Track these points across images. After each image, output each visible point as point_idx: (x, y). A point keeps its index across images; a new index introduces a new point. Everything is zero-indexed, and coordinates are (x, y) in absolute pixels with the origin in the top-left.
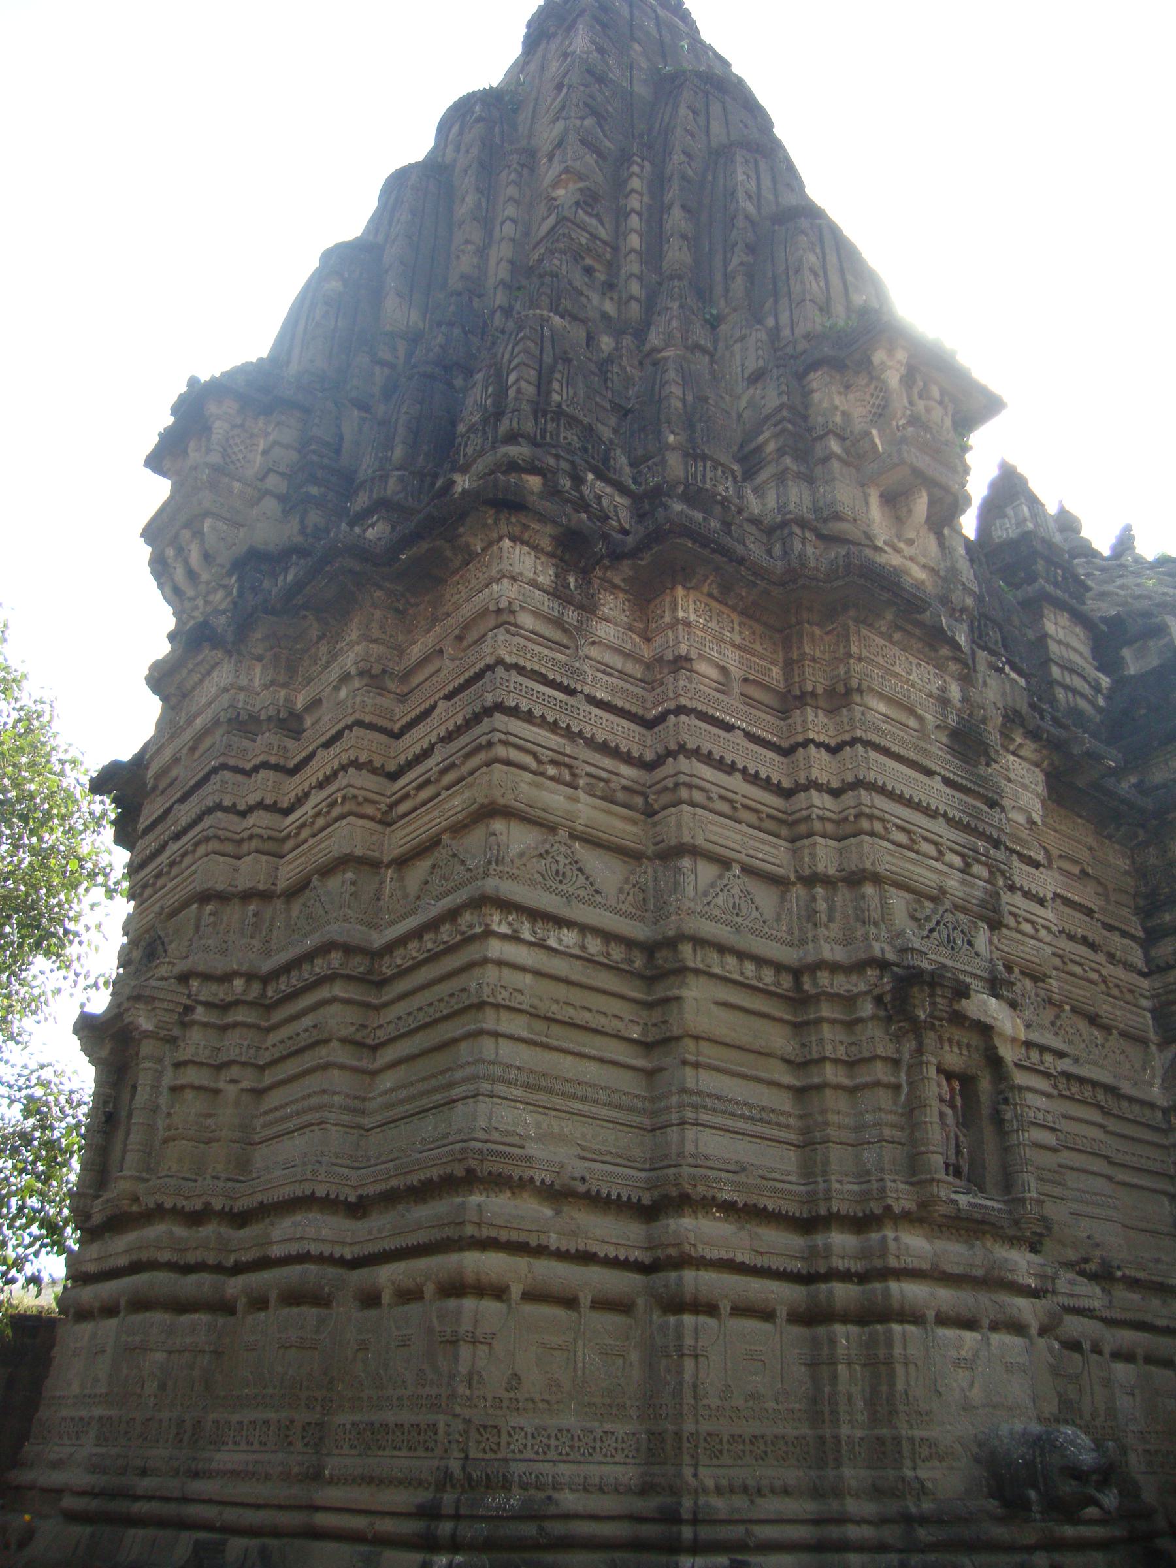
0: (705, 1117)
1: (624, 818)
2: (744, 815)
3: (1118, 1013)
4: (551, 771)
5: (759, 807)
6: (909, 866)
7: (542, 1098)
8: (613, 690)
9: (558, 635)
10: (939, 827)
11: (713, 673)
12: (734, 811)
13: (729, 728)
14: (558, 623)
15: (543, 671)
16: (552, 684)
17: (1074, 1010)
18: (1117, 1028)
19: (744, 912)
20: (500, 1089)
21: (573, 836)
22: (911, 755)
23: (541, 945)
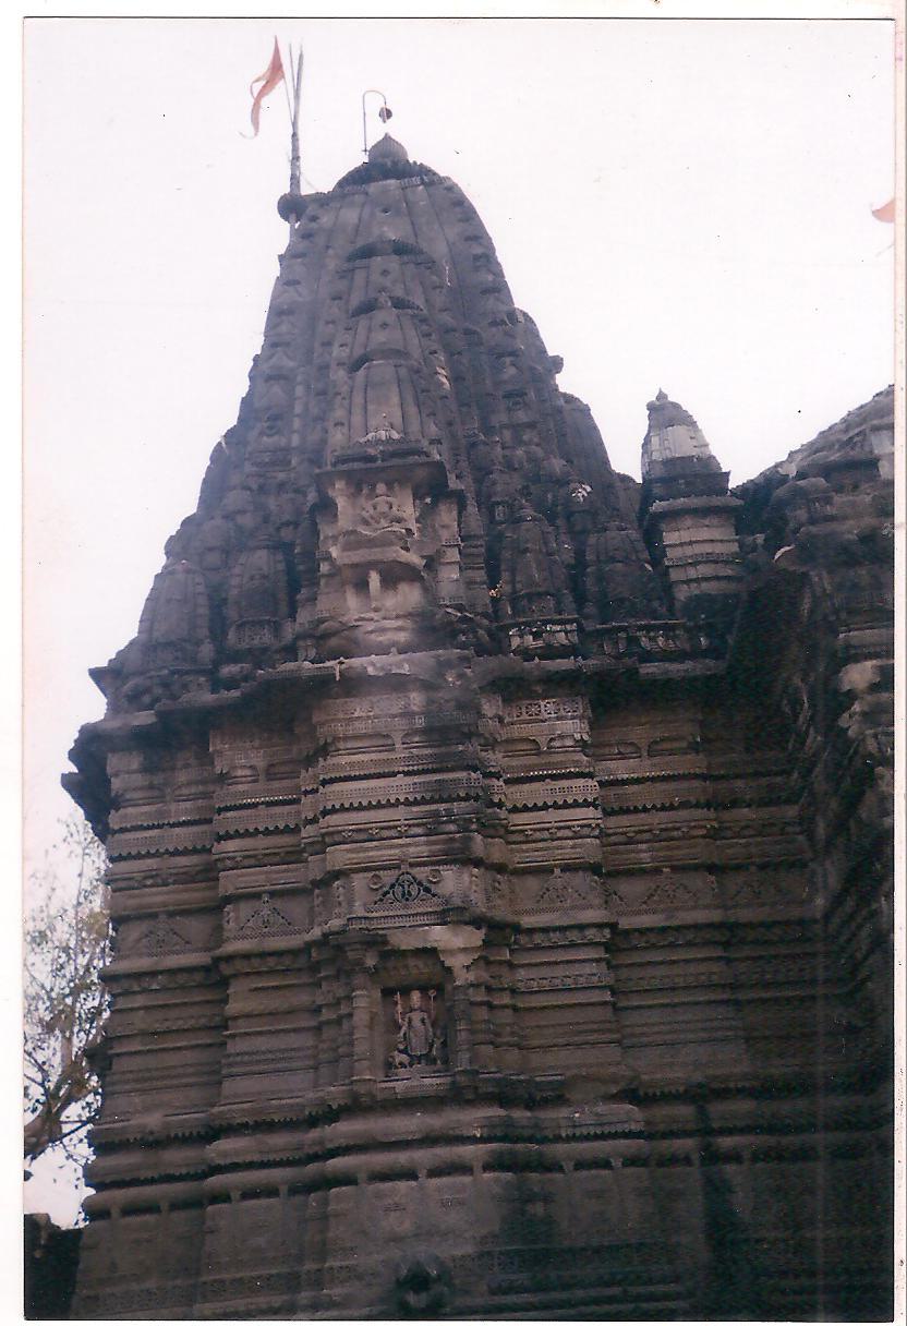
0: (235, 1070)
1: (204, 889)
2: (246, 862)
3: (753, 850)
4: (149, 882)
5: (277, 851)
6: (371, 854)
7: (146, 1085)
8: (186, 812)
9: (156, 793)
10: (400, 814)
11: (248, 772)
12: (259, 861)
13: (255, 805)
14: (151, 787)
15: (139, 823)
16: (149, 828)
17: (674, 869)
18: (753, 863)
19: (272, 922)
20: (235, 1070)
21: (171, 914)
22: (373, 771)
23: (144, 991)
